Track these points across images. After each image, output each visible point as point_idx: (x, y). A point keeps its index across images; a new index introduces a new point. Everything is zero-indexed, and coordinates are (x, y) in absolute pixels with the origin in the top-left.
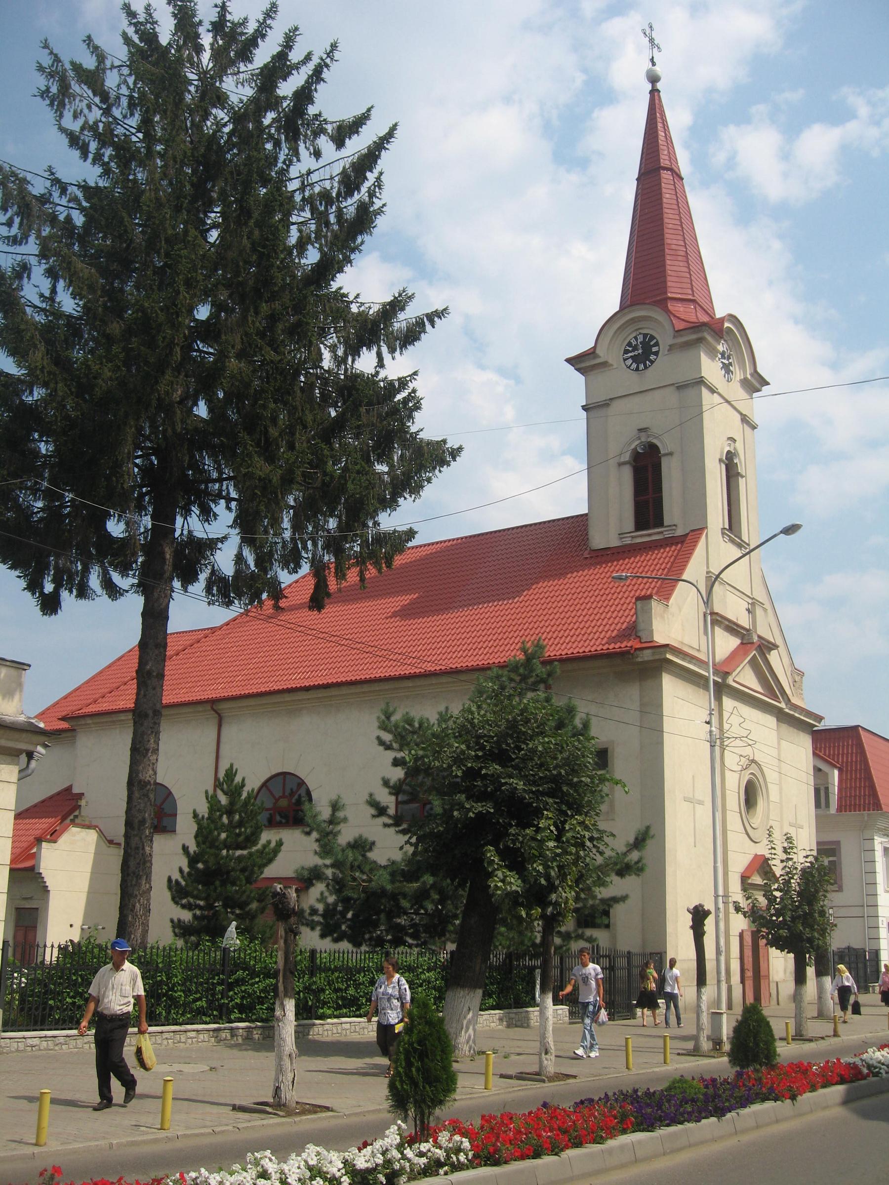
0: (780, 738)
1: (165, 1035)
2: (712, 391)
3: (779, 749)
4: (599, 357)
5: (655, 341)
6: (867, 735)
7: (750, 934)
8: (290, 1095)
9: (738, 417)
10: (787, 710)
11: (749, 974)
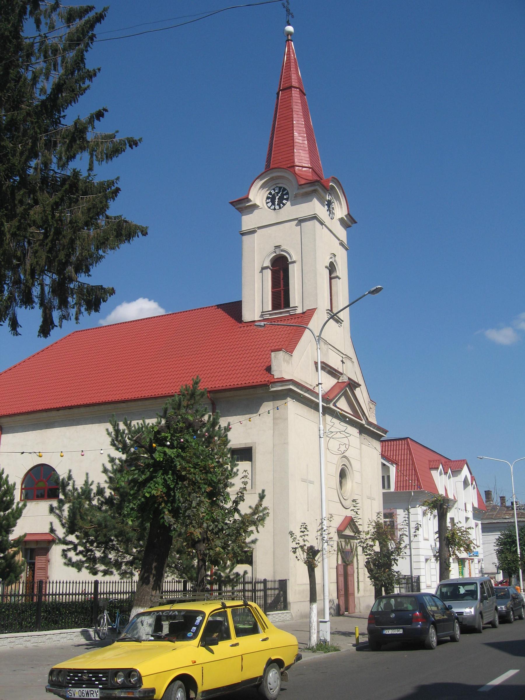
0: (361, 443)
1: (47, 637)
2: (322, 223)
3: (360, 449)
5: (286, 191)
6: (413, 443)
8: (333, 280)
9: (338, 242)
10: (366, 426)
11: (342, 592)
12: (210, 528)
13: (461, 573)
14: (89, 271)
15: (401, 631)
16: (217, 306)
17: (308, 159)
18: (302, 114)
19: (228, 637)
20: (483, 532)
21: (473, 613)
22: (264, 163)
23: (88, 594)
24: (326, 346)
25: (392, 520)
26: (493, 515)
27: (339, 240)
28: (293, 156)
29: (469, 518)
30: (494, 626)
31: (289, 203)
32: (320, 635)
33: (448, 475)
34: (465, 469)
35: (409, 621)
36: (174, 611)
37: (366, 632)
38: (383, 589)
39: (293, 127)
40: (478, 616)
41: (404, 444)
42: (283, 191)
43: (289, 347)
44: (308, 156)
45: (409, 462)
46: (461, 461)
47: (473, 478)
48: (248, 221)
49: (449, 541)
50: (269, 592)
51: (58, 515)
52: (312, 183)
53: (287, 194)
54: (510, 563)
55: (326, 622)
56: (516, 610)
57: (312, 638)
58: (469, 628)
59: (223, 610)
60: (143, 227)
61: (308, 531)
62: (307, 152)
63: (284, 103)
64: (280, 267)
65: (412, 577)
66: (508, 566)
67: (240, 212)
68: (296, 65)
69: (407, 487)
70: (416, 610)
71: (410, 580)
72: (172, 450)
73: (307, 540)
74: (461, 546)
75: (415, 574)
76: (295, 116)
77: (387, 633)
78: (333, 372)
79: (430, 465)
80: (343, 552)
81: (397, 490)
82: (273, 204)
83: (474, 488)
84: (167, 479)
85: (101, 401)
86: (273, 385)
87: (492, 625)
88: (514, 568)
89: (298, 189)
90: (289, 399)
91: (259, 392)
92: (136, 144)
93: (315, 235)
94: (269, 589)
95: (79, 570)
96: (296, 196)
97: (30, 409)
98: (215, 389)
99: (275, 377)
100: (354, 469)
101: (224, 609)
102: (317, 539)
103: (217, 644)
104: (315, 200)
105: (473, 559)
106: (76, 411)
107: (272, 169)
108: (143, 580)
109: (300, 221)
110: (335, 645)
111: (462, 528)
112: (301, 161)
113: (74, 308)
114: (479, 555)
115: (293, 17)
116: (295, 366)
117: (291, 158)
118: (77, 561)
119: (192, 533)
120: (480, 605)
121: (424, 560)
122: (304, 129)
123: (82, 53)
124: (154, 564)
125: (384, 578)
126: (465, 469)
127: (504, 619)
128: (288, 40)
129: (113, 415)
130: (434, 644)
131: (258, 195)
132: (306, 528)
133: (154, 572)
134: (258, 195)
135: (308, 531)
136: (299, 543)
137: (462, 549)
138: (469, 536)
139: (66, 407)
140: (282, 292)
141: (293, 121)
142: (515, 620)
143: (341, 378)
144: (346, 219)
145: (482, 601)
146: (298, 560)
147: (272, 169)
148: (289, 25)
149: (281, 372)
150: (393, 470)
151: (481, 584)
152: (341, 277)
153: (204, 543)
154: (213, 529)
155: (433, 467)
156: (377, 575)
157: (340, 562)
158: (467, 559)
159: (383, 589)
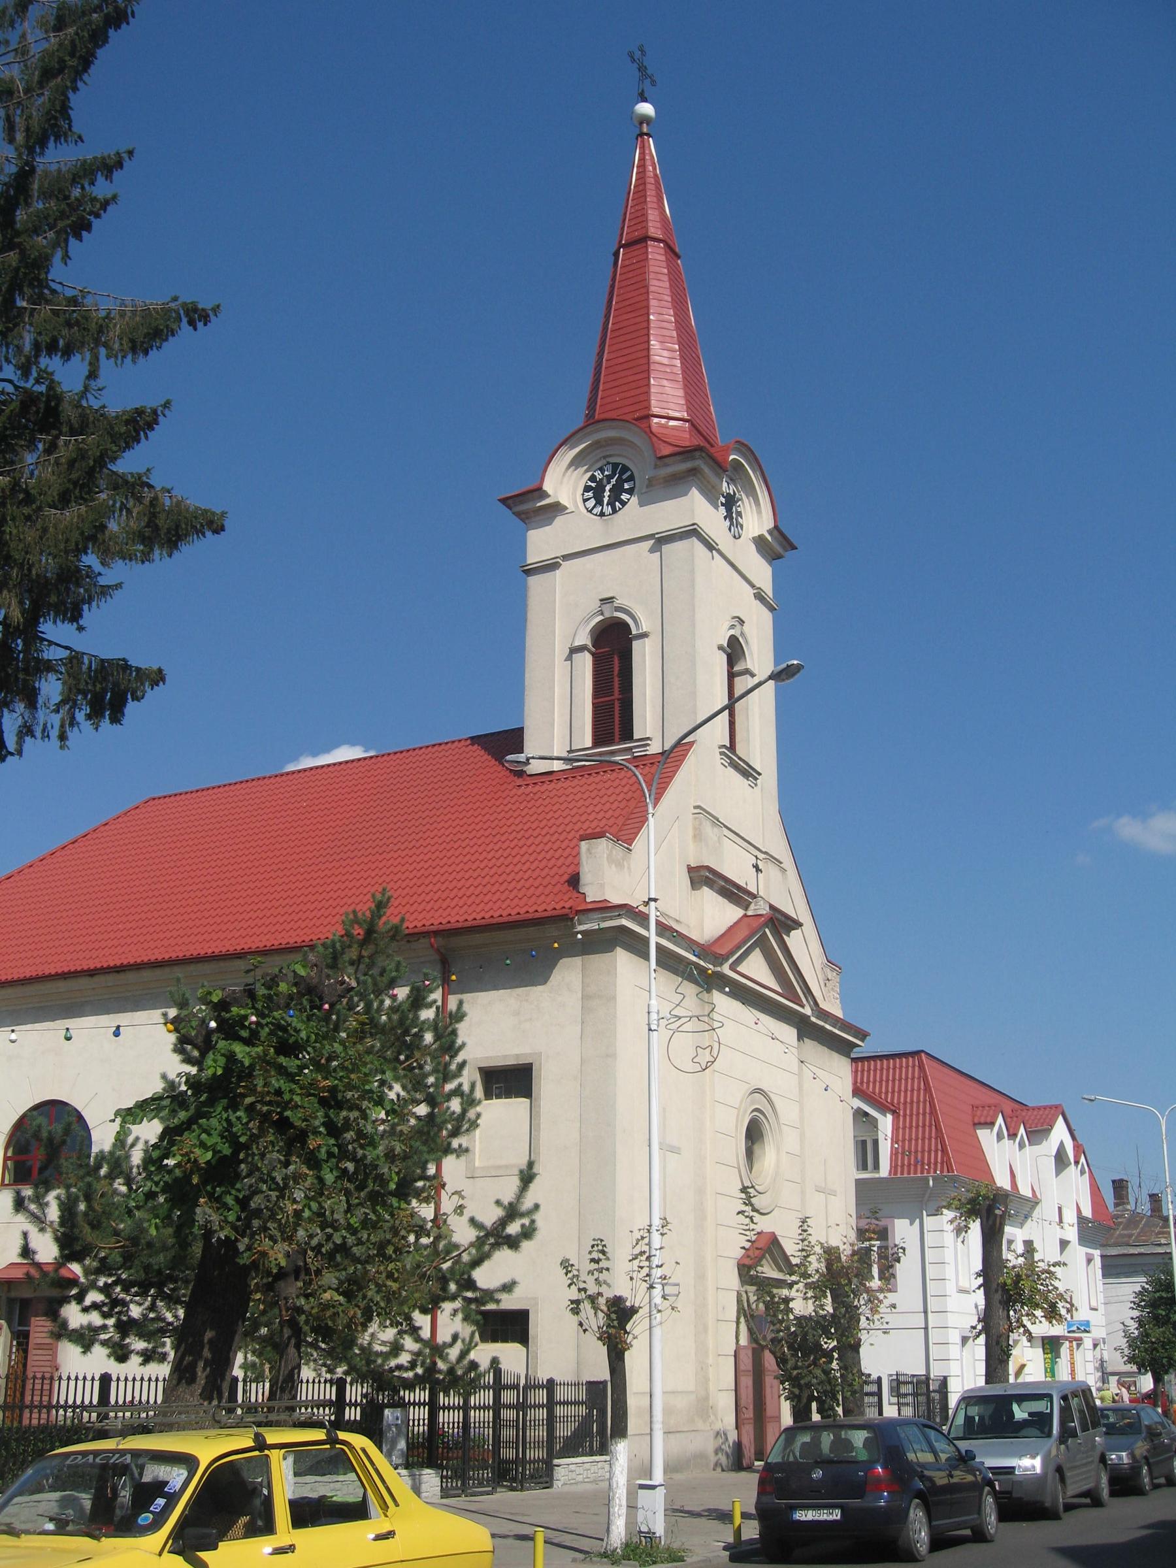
2: (710, 546)
4: (548, 496)
5: (629, 473)
7: (750, 1353)
9: (752, 591)
10: (813, 1019)
11: (749, 1414)
12: (314, 1242)
13: (1051, 1371)
14: (81, 616)
15: (836, 1515)
16: (472, 738)
17: (683, 402)
18: (669, 299)
19: (269, 1528)
20: (1104, 1276)
21: (1038, 1470)
22: (583, 411)
23: (83, 1407)
24: (716, 830)
25: (884, 1243)
26: (1130, 1236)
27: (753, 586)
28: (648, 393)
29: (1068, 1242)
30: (1097, 1503)
31: (634, 500)
32: (640, 1518)
33: (1018, 1140)
34: (1060, 1126)
35: (859, 1489)
36: (123, 1452)
37: (754, 1511)
38: (814, 1405)
39: (648, 328)
40: (1053, 1477)
41: (914, 1067)
42: (621, 474)
43: (625, 827)
44: (681, 393)
45: (924, 1109)
46: (1051, 1107)
47: (1079, 1149)
48: (541, 543)
49: (1009, 1293)
50: (559, 1411)
51: (33, 1215)
52: (686, 453)
53: (631, 478)
54: (1155, 1349)
55: (653, 1487)
56: (1158, 1463)
57: (613, 1528)
58: (1021, 1505)
59: (257, 1453)
60: (214, 514)
61: (608, 1259)
62: (681, 385)
63: (631, 275)
64: (612, 645)
65: (928, 1377)
66: (1151, 1352)
67: (523, 520)
68: (658, 189)
69: (919, 1167)
70: (877, 1461)
71: (924, 1386)
72: (248, 1049)
73: (605, 1282)
74: (1037, 1306)
75: (936, 1372)
76: (653, 303)
77: (803, 1518)
78: (733, 892)
79: (974, 1116)
80: (752, 1316)
81: (896, 1173)
82: (599, 502)
83: (1082, 1172)
84: (234, 1120)
85: (188, 954)
86: (583, 917)
87: (1093, 1499)
88: (1165, 1361)
89: (656, 467)
90: (619, 949)
91: (544, 934)
92: (205, 318)
93: (692, 571)
94: (560, 1403)
95: (87, 1348)
96: (650, 483)
97: (28, 972)
98: (449, 926)
99: (588, 900)
100: (782, 1121)
101: (261, 1449)
102: (632, 1279)
103: (216, 1548)
104: (695, 494)
105: (1080, 1339)
106: (131, 976)
107: (598, 421)
108: (182, 1373)
109: (661, 541)
110: (675, 1546)
111: (1040, 1264)
112: (664, 405)
113: (58, 711)
114: (1092, 1328)
115: (653, 83)
116: (631, 874)
117: (641, 398)
118: (82, 1327)
119: (264, 1254)
120: (1058, 1449)
121: (958, 1340)
122: (674, 334)
123: (64, 94)
124: (209, 1335)
125: (814, 1381)
126: (1060, 1126)
127: (1125, 1484)
128: (642, 134)
129: (178, 980)
130: (923, 1546)
131: (564, 483)
132: (603, 1252)
133: (207, 1353)
134: (564, 483)
135: (608, 1259)
136: (585, 1290)
137: (1039, 1313)
138: (1056, 1283)
139: (109, 967)
140: (617, 704)
141: (648, 315)
142: (1156, 1487)
143: (752, 907)
144: (769, 538)
145: (1062, 1439)
146: (585, 1331)
147: (598, 421)
148: (645, 100)
149: (602, 886)
150: (886, 1123)
151: (1065, 1398)
152: (756, 672)
153: (297, 1279)
154: (320, 1245)
155: (982, 1120)
156: (795, 1372)
157: (744, 1341)
158: (1066, 1338)
159: (814, 1405)
